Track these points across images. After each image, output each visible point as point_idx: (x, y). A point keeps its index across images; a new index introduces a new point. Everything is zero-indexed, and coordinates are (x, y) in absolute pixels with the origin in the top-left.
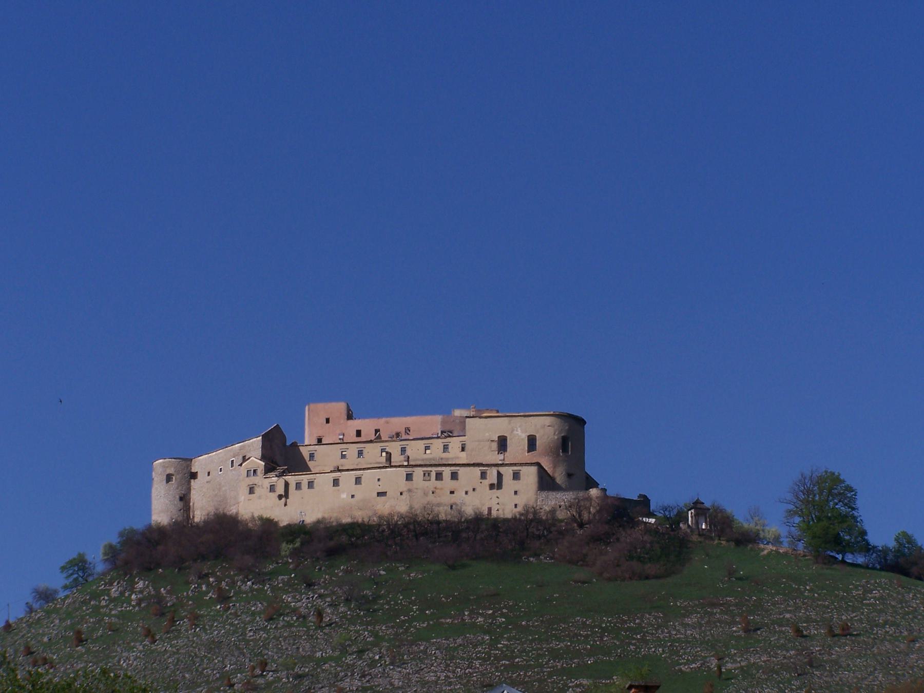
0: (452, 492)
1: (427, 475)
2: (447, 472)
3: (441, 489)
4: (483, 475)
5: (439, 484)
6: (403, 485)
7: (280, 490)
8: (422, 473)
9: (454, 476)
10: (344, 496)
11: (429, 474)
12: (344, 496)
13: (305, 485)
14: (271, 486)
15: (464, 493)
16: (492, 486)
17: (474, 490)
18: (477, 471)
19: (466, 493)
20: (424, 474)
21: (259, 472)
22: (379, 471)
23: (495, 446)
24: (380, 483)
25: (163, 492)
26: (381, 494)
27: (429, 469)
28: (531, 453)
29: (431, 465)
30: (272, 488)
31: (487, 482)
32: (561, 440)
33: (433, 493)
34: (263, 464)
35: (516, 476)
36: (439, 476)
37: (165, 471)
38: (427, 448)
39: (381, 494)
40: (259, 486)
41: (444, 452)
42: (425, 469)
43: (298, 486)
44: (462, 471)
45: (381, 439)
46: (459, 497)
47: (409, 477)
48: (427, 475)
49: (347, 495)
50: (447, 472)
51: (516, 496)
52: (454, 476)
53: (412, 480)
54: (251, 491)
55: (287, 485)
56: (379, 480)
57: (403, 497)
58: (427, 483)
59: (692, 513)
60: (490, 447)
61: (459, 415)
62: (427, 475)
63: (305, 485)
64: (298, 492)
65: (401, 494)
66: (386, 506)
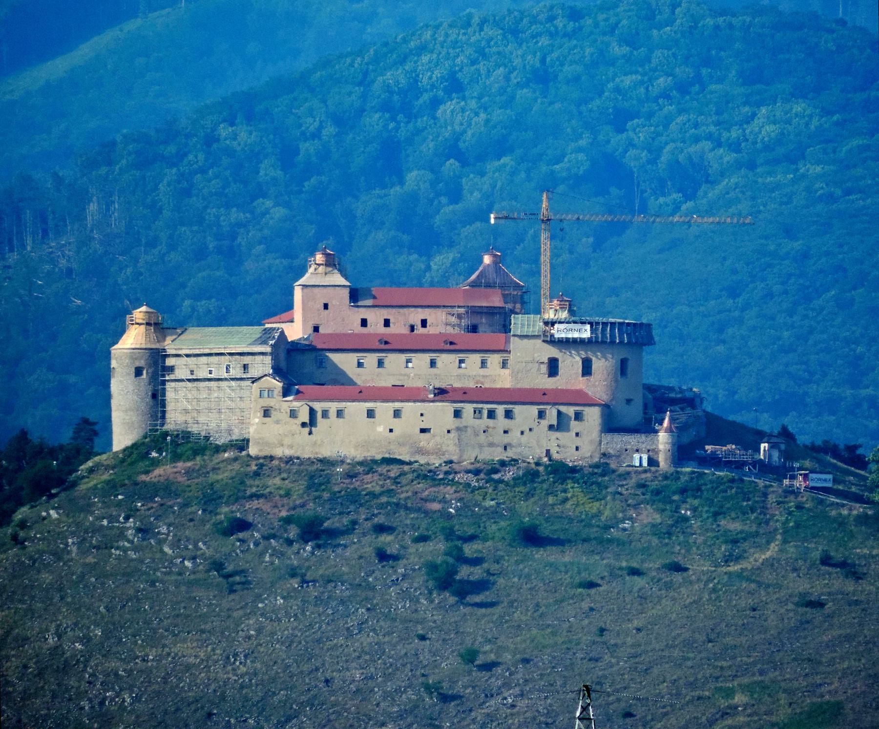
0: (506, 432)
1: (477, 412)
2: (500, 410)
3: (494, 428)
4: (541, 415)
5: (491, 422)
6: (450, 421)
7: (305, 417)
8: (472, 410)
9: (508, 414)
10: (380, 429)
11: (480, 412)
12: (380, 429)
13: (333, 413)
14: (291, 410)
15: (519, 433)
16: (551, 427)
17: (530, 430)
18: (534, 410)
19: (522, 433)
20: (475, 412)
21: (276, 392)
22: (446, 406)
23: (544, 368)
24: (423, 418)
25: (131, 388)
26: (423, 431)
27: (480, 406)
28: (585, 378)
29: (482, 402)
30: (293, 414)
31: (545, 423)
32: (620, 362)
33: (484, 432)
34: (280, 385)
35: (578, 416)
36: (491, 414)
37: (134, 363)
38: (408, 361)
39: (423, 431)
40: (276, 409)
41: (482, 367)
42: (475, 405)
43: (325, 414)
44: (517, 409)
45: (659, 466)
46: (514, 437)
47: (457, 414)
48: (477, 412)
49: (384, 429)
50: (500, 410)
51: (577, 438)
52: (508, 414)
53: (461, 418)
54: (266, 413)
55: (312, 412)
56: (422, 415)
57: (452, 435)
58: (478, 422)
59: (765, 447)
60: (539, 370)
61: (808, 443)
62: (477, 412)
63: (333, 413)
64: (325, 420)
65: (449, 432)
66: (431, 445)
